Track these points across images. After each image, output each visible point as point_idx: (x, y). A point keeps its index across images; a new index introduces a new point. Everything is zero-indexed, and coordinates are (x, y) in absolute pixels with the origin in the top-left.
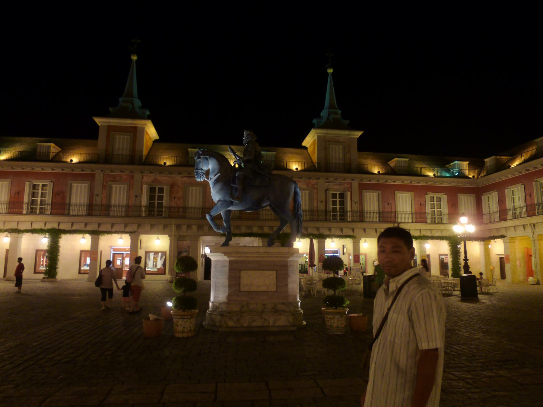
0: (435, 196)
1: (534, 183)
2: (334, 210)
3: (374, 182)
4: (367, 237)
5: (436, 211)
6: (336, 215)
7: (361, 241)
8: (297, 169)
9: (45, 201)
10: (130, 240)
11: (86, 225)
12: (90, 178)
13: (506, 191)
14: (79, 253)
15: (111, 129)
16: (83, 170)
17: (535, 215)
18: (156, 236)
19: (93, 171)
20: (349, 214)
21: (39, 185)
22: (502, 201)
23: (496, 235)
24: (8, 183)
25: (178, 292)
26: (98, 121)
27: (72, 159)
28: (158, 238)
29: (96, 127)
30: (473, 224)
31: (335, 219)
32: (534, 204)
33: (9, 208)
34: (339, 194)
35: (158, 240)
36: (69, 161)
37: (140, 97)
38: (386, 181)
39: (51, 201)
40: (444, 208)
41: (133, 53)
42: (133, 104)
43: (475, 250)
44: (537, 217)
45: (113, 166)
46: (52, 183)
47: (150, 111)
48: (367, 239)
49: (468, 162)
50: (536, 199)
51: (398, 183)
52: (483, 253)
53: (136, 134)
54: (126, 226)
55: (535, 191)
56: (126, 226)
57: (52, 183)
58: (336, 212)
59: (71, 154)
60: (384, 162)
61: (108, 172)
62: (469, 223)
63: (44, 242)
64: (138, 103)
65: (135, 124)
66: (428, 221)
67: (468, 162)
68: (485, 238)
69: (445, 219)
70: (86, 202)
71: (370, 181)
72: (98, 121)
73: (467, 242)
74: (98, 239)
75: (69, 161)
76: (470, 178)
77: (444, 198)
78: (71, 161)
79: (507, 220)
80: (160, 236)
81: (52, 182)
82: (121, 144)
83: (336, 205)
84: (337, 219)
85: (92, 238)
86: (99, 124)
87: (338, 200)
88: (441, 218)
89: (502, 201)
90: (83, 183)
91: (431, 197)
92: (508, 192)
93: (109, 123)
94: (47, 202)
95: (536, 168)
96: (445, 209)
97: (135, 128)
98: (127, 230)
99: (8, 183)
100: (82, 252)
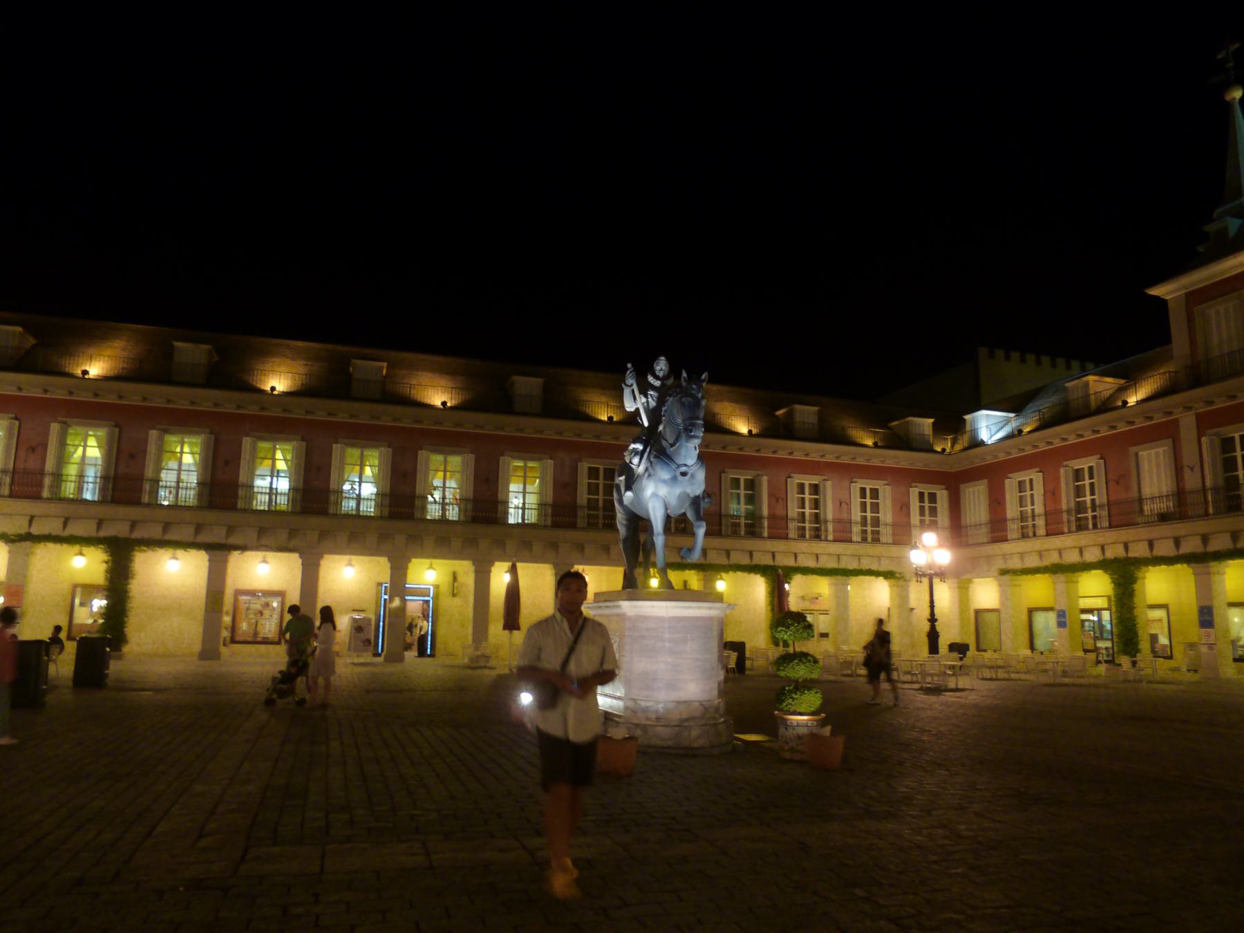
0: (807, 483)
1: (1062, 471)
2: (802, 517)
3: (733, 451)
4: (435, 557)
5: (807, 514)
6: (597, 516)
7: (493, 569)
8: (444, 403)
10: (207, 564)
11: (100, 524)
12: (1166, 431)
13: (1007, 481)
14: (1025, 612)
15: (1195, 298)
16: (96, 395)
17: (1063, 533)
18: (427, 561)
20: (830, 527)
22: (996, 501)
23: (874, 567)
25: (515, 671)
28: (264, 561)
29: (1161, 303)
30: (947, 547)
31: (592, 525)
32: (1061, 512)
33: (391, 505)
34: (810, 485)
35: (264, 565)
36: (79, 372)
38: (774, 452)
39: (11, 466)
40: (885, 515)
43: (945, 595)
44: (1062, 538)
45: (356, 406)
46: (17, 423)
48: (434, 561)
49: (932, 420)
50: (1064, 501)
51: (782, 455)
52: (772, 603)
54: (199, 528)
55: (1063, 485)
56: (199, 528)
57: (17, 423)
58: (597, 509)
59: (91, 359)
60: (761, 410)
62: (940, 546)
63: (86, 564)
66: (855, 538)
67: (932, 420)
68: (961, 576)
69: (886, 534)
71: (598, 437)
72: (1155, 291)
73: (936, 581)
74: (225, 562)
75: (79, 372)
77: (942, 495)
78: (85, 372)
79: (1007, 540)
80: (355, 558)
81: (16, 418)
84: (597, 524)
85: (10, 552)
87: (601, 482)
88: (878, 532)
89: (996, 501)
91: (590, 468)
92: (1010, 484)
93: (1185, 287)
95: (1066, 440)
96: (887, 514)
98: (201, 538)
100: (75, 586)
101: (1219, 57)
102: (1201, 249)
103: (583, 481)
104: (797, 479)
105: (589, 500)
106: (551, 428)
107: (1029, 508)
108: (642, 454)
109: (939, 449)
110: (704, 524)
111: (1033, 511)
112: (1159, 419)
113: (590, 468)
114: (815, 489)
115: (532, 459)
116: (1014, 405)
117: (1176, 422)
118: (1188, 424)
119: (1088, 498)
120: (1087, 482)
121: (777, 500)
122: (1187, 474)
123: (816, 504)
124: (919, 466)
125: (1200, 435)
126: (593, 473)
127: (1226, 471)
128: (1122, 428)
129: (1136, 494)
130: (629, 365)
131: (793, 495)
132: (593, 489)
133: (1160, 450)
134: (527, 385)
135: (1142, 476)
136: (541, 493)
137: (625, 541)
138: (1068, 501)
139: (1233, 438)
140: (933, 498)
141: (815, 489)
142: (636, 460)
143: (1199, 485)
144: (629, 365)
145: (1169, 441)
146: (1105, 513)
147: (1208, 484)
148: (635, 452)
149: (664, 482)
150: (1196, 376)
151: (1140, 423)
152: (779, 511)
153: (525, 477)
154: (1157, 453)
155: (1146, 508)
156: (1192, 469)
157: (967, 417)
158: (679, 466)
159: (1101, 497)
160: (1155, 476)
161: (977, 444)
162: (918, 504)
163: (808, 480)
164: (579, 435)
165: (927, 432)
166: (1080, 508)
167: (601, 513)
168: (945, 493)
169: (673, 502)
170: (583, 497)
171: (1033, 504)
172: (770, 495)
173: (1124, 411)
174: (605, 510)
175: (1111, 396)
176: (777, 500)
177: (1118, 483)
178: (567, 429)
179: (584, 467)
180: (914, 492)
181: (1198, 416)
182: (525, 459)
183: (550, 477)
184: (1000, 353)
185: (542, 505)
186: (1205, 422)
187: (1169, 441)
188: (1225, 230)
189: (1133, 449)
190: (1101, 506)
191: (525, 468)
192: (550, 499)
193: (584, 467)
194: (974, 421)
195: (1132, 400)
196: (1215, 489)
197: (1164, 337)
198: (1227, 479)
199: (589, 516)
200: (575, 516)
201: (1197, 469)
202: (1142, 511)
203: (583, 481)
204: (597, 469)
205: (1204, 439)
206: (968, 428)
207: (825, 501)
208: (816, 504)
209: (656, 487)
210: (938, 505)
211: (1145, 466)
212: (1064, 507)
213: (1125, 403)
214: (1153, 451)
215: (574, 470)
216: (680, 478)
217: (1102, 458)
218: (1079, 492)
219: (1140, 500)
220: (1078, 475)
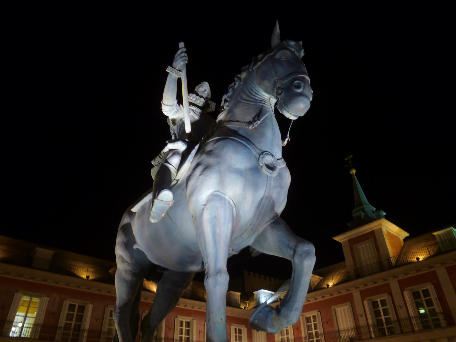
5: (183, 338)
9: (389, 318)
12: (347, 299)
15: (352, 242)
19: (348, 290)
21: (310, 317)
24: (348, 306)
26: (338, 239)
27: (419, 257)
29: (339, 244)
36: (415, 260)
37: (372, 203)
41: (350, 169)
42: (364, 211)
47: (385, 211)
49: (239, 294)
53: (375, 238)
61: (401, 277)
64: (370, 208)
65: (370, 228)
67: (239, 294)
70: (352, 324)
72: (338, 239)
75: (415, 260)
76: (242, 309)
77: (244, 330)
78: (418, 259)
82: (366, 253)
83: (383, 310)
86: (340, 242)
90: (341, 306)
91: (70, 305)
93: (348, 237)
94: (319, 333)
97: (373, 232)
99: (348, 306)
101: (346, 159)
102: (349, 225)
103: (65, 311)
104: (180, 318)
105: (66, 323)
106: (52, 279)
107: (286, 337)
108: (184, 156)
109: (243, 307)
110: (311, 248)
111: (288, 338)
112: (344, 293)
113: (70, 305)
114: (188, 324)
115: (37, 296)
116: (274, 289)
117: (351, 294)
118: (357, 295)
119: (314, 331)
120: (313, 323)
121: (169, 329)
122: (399, 310)
123: (188, 332)
124: (235, 315)
125: (363, 300)
126: (72, 307)
127: (376, 317)
128: (328, 297)
129: (336, 329)
130: (182, 45)
131: (177, 327)
132: (70, 317)
133: (345, 307)
134: (44, 253)
135: (338, 320)
136: (37, 318)
137: (123, 308)
138: (305, 332)
139: (377, 302)
140: (240, 331)
141: (188, 324)
142: (175, 161)
143: (366, 323)
144: (182, 45)
145: (349, 303)
146: (323, 338)
147: (370, 322)
148: (174, 152)
149: (239, 172)
150: (358, 274)
151: (336, 295)
152: (170, 336)
153: (28, 307)
154: (344, 310)
155: (342, 335)
156: (361, 316)
157: (255, 293)
158: (263, 153)
159: (320, 330)
160: (344, 320)
161: (258, 304)
162: (234, 334)
163: (185, 319)
164: (68, 285)
165: (237, 299)
166: (310, 336)
167: (71, 332)
168: (246, 329)
169: (248, 211)
170: (62, 322)
171: (287, 334)
172: (166, 326)
173: (328, 289)
174: (74, 330)
175: (319, 283)
176: (169, 329)
177: (327, 323)
178: (61, 280)
179: (67, 303)
180: (233, 328)
181: (360, 291)
182: (31, 296)
183: (45, 308)
184: (252, 274)
185: (36, 325)
186: (364, 294)
187: (349, 303)
188: (360, 216)
189: (333, 307)
190: (321, 335)
191: (30, 302)
192: (41, 322)
193: (67, 303)
194: (258, 295)
195: (331, 284)
196: (373, 325)
197: (341, 258)
198: (309, 334)
199: (64, 334)
200: (56, 333)
201: (364, 316)
202: (340, 337)
203: (65, 311)
204: (75, 306)
205: (365, 302)
206: (255, 297)
207: (193, 330)
208: (188, 332)
209: (221, 183)
210: (243, 335)
211: (339, 315)
212: (303, 335)
213: (328, 286)
214: (342, 308)
215: (61, 304)
216: (265, 171)
217: (319, 311)
218: (309, 328)
219: (339, 332)
220: (308, 320)
